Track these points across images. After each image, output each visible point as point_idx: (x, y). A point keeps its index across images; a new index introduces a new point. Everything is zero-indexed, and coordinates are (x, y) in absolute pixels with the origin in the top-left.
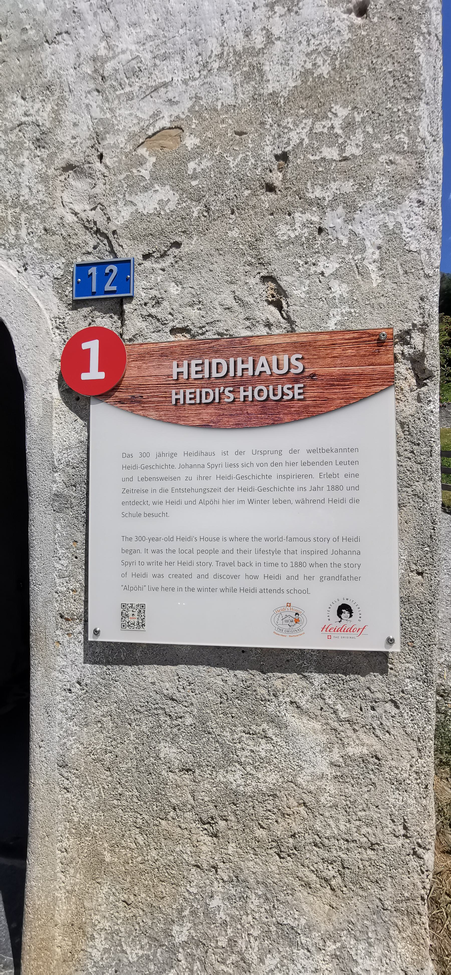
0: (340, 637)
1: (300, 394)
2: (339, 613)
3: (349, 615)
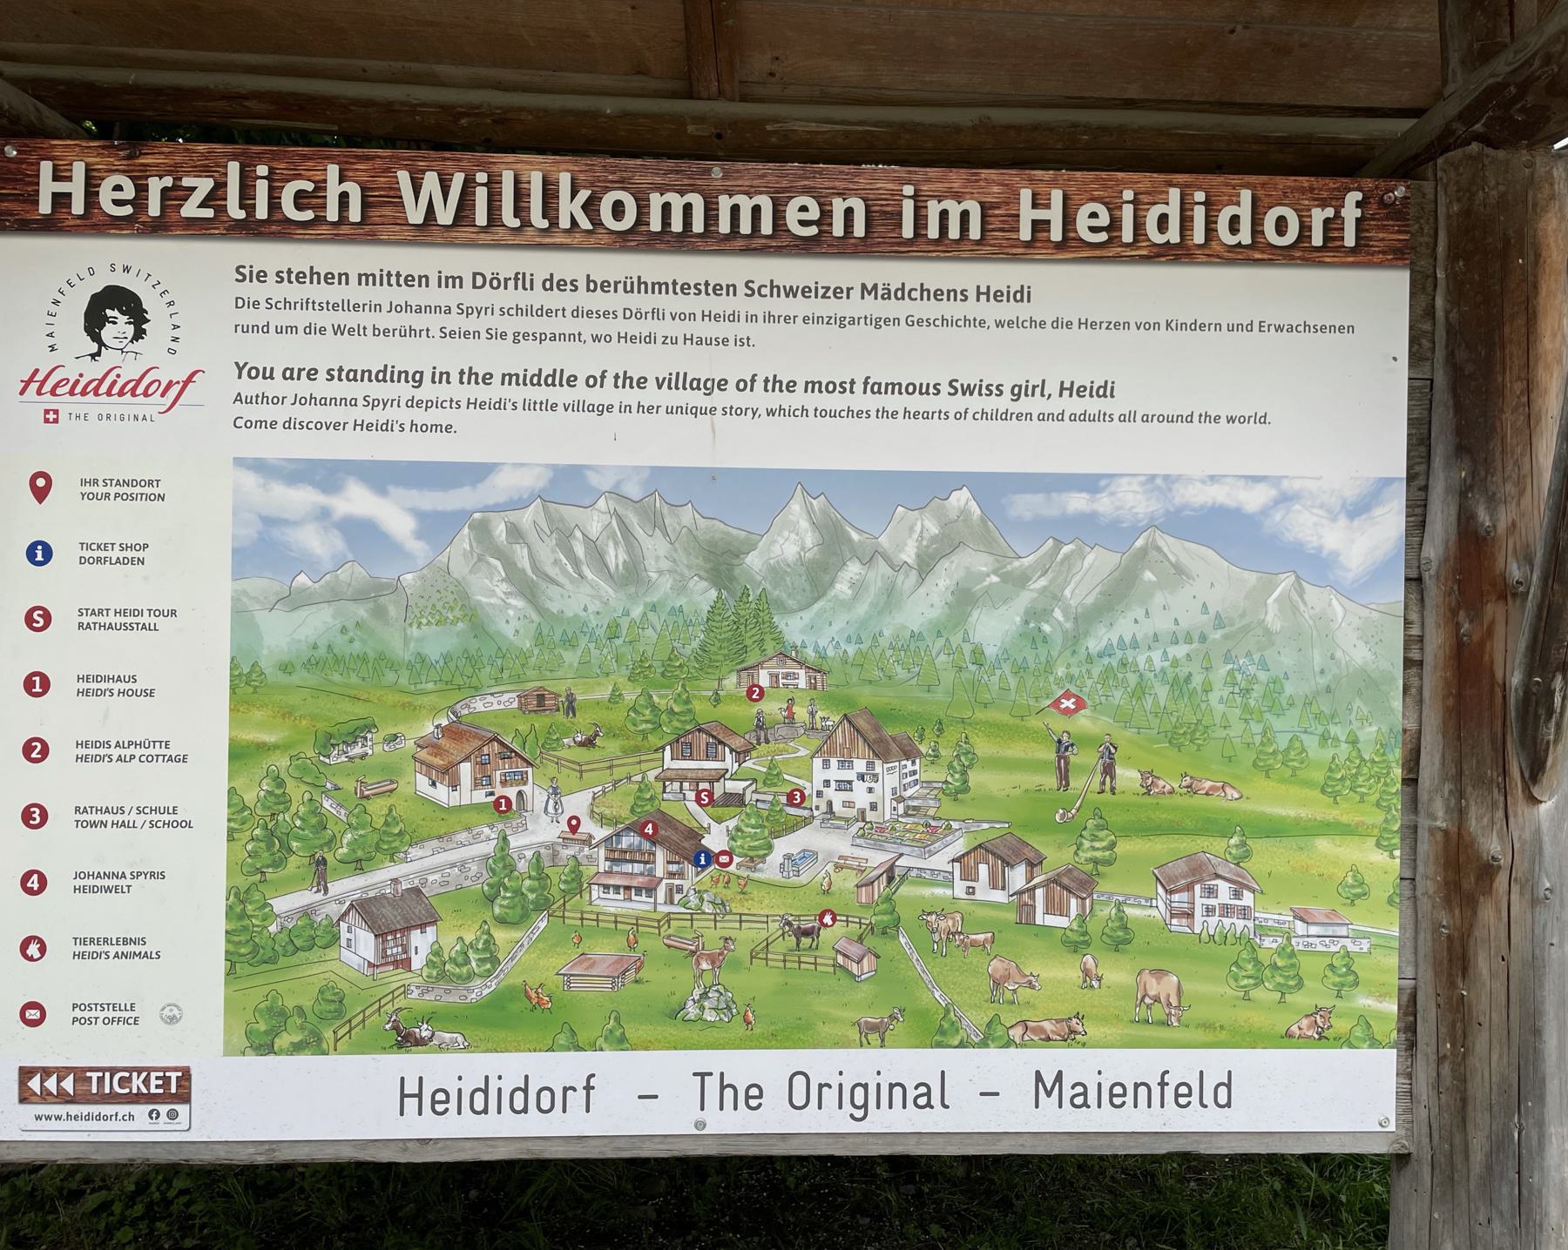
0: (93, 417)
1: (157, 1087)
2: (94, 321)
3: (130, 330)
